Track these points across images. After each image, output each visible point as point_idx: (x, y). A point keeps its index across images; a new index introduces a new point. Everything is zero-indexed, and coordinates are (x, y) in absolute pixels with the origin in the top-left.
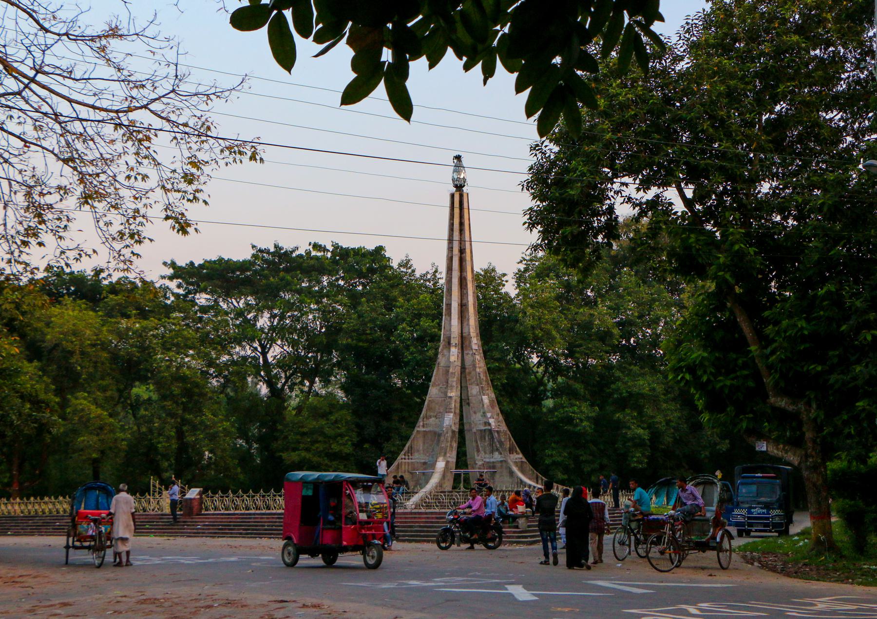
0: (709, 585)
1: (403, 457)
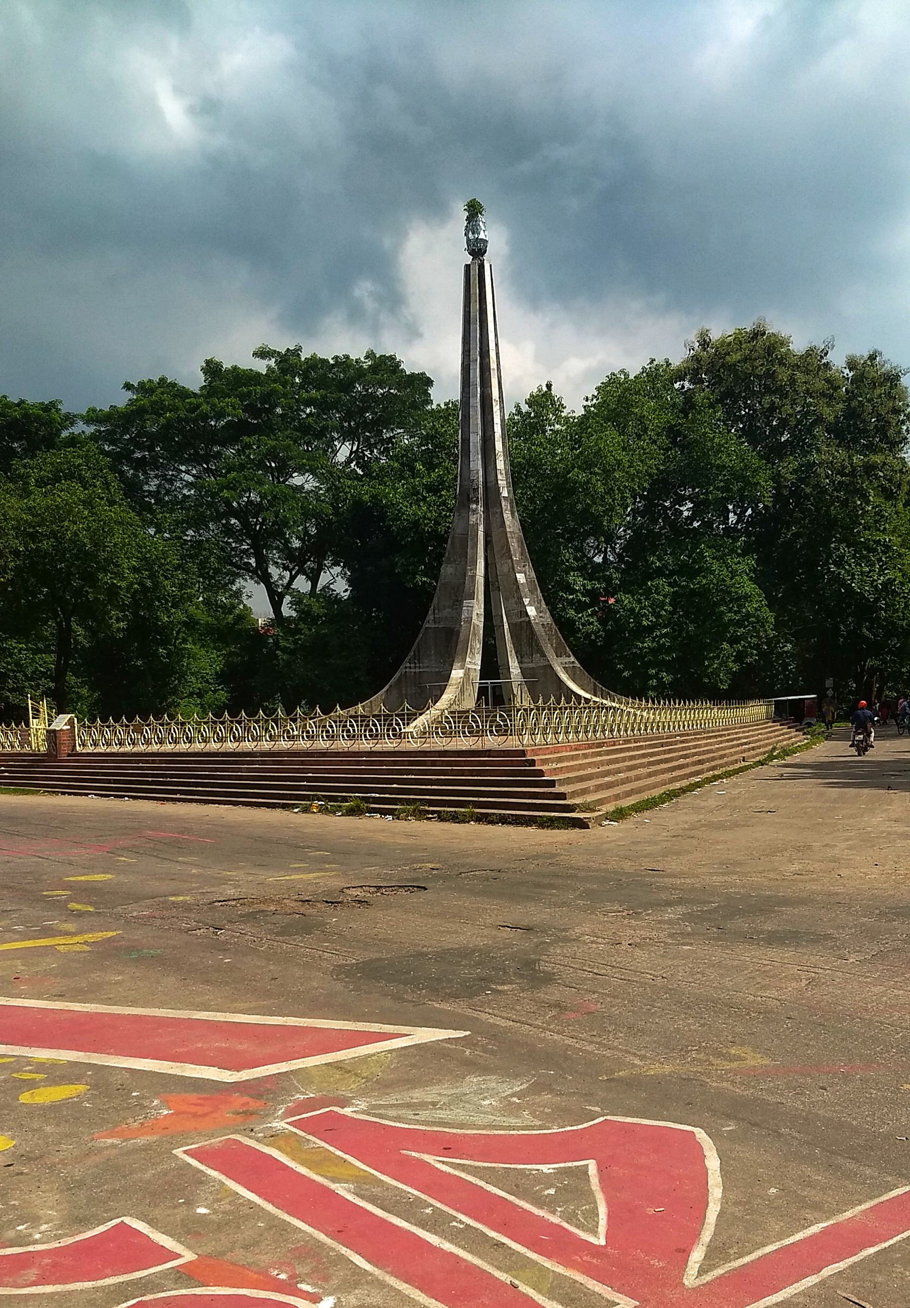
0: (486, 799)
1: (408, 665)
